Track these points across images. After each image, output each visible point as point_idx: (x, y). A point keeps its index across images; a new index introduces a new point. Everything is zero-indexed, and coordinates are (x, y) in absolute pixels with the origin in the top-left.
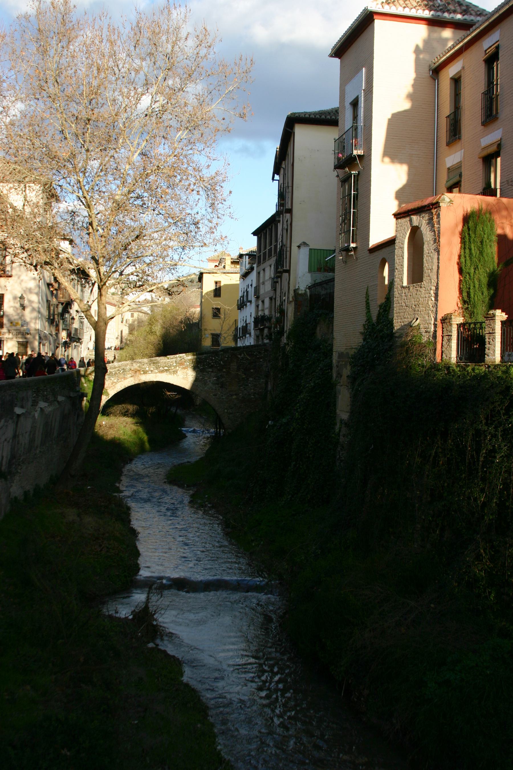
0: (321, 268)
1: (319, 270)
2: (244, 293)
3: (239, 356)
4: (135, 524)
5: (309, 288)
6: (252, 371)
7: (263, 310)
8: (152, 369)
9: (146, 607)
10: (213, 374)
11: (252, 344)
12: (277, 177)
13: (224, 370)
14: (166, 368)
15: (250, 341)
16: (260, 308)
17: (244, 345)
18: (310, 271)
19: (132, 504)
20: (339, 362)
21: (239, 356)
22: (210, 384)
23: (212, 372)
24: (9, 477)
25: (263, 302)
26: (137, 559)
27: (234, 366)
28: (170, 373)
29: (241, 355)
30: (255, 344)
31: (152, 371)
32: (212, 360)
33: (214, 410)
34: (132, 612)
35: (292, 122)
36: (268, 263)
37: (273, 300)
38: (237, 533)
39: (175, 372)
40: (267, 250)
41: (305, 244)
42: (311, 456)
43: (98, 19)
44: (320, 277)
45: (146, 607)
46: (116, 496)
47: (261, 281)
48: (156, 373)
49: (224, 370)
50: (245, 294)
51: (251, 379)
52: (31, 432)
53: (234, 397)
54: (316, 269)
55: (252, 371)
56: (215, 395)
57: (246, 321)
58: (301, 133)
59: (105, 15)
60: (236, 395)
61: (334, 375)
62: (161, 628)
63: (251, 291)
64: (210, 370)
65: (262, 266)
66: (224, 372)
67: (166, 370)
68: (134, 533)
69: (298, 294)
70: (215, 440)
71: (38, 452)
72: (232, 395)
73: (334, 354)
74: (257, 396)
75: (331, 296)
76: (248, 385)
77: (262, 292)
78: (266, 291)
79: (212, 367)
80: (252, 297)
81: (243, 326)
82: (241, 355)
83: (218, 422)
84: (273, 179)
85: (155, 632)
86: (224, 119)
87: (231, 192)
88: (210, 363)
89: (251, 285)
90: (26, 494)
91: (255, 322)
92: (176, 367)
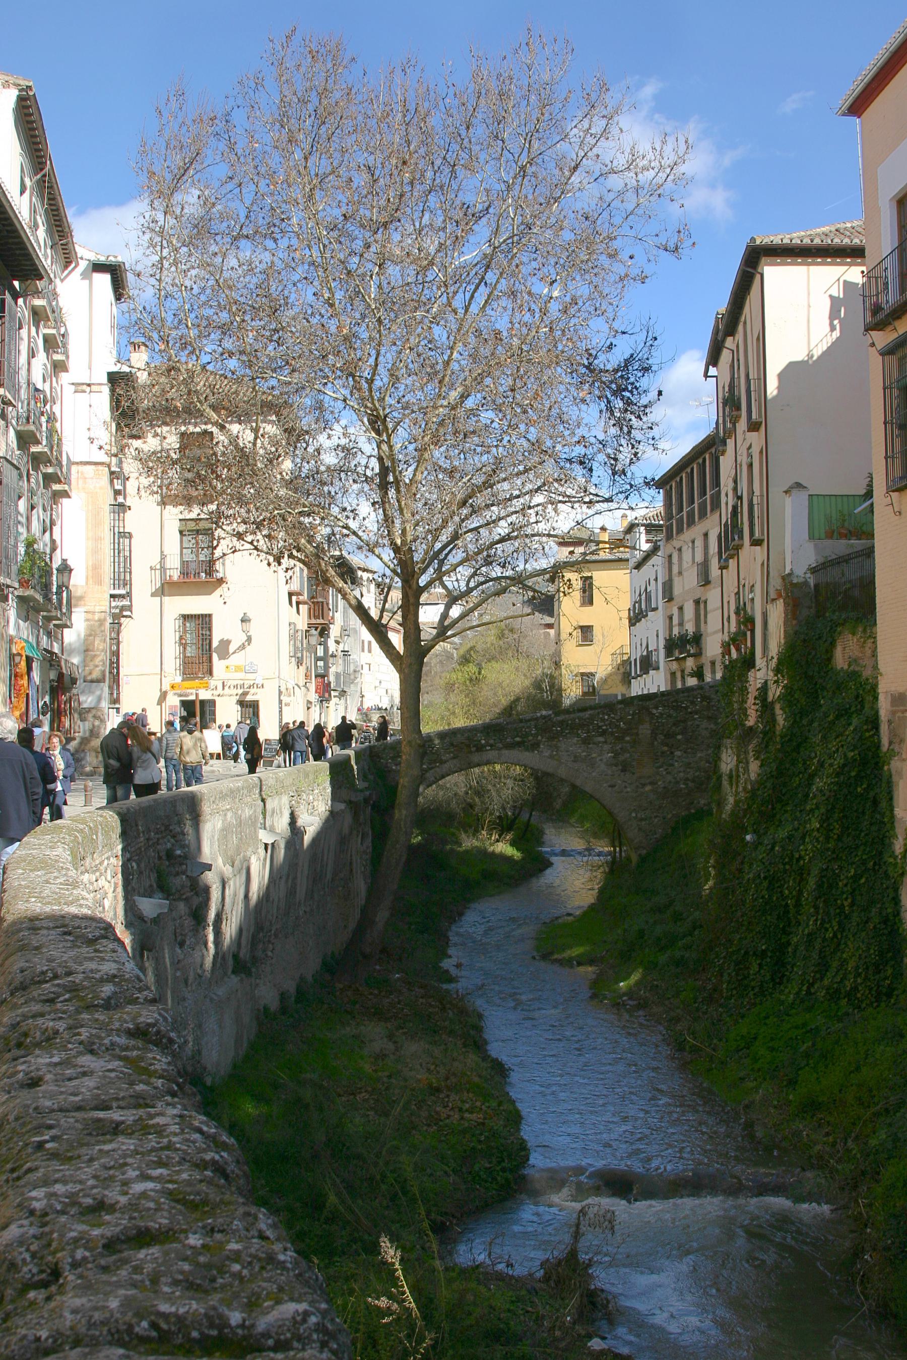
0: (833, 532)
1: (830, 535)
2: (640, 595)
3: (654, 711)
4: (496, 1050)
5: (814, 570)
6: (679, 737)
7: (681, 624)
8: (491, 742)
9: (573, 1254)
10: (606, 747)
11: (663, 689)
12: (713, 371)
13: (627, 738)
14: (518, 739)
15: (655, 682)
16: (675, 621)
17: (645, 692)
18: (811, 537)
19: (479, 1003)
20: (894, 713)
21: (654, 711)
22: (603, 767)
23: (605, 742)
24: (253, 970)
25: (681, 609)
26: (518, 1130)
27: (645, 730)
28: (527, 750)
29: (657, 708)
30: (669, 688)
31: (491, 746)
32: (603, 720)
33: (611, 814)
34: (542, 1265)
35: (755, 257)
36: (688, 535)
37: (702, 606)
38: (701, 1060)
39: (535, 746)
40: (684, 513)
41: (799, 485)
42: (846, 903)
43: (398, 71)
44: (841, 547)
45: (573, 1254)
46: (447, 991)
47: (675, 569)
48: (500, 749)
49: (627, 738)
50: (643, 597)
51: (678, 753)
52: (288, 876)
53: (648, 788)
54: (823, 536)
55: (679, 737)
56: (612, 786)
57: (647, 647)
58: (776, 277)
59: (413, 62)
60: (650, 783)
61: (885, 742)
62: (604, 1296)
63: (656, 591)
64: (601, 739)
65: (676, 543)
66: (628, 742)
67: (519, 744)
68: (500, 1070)
69: (792, 584)
70: (615, 868)
71: (301, 913)
72: (644, 785)
73: (881, 697)
74: (690, 784)
75: (868, 585)
76: (672, 765)
77: (677, 591)
78: (686, 588)
79: (603, 733)
80: (658, 599)
81: (642, 656)
82: (657, 708)
83: (617, 836)
84: (706, 376)
85: (597, 1308)
86: (631, 257)
87: (660, 393)
88: (600, 727)
89: (656, 580)
90: (283, 996)
91: (666, 647)
92: (536, 735)
